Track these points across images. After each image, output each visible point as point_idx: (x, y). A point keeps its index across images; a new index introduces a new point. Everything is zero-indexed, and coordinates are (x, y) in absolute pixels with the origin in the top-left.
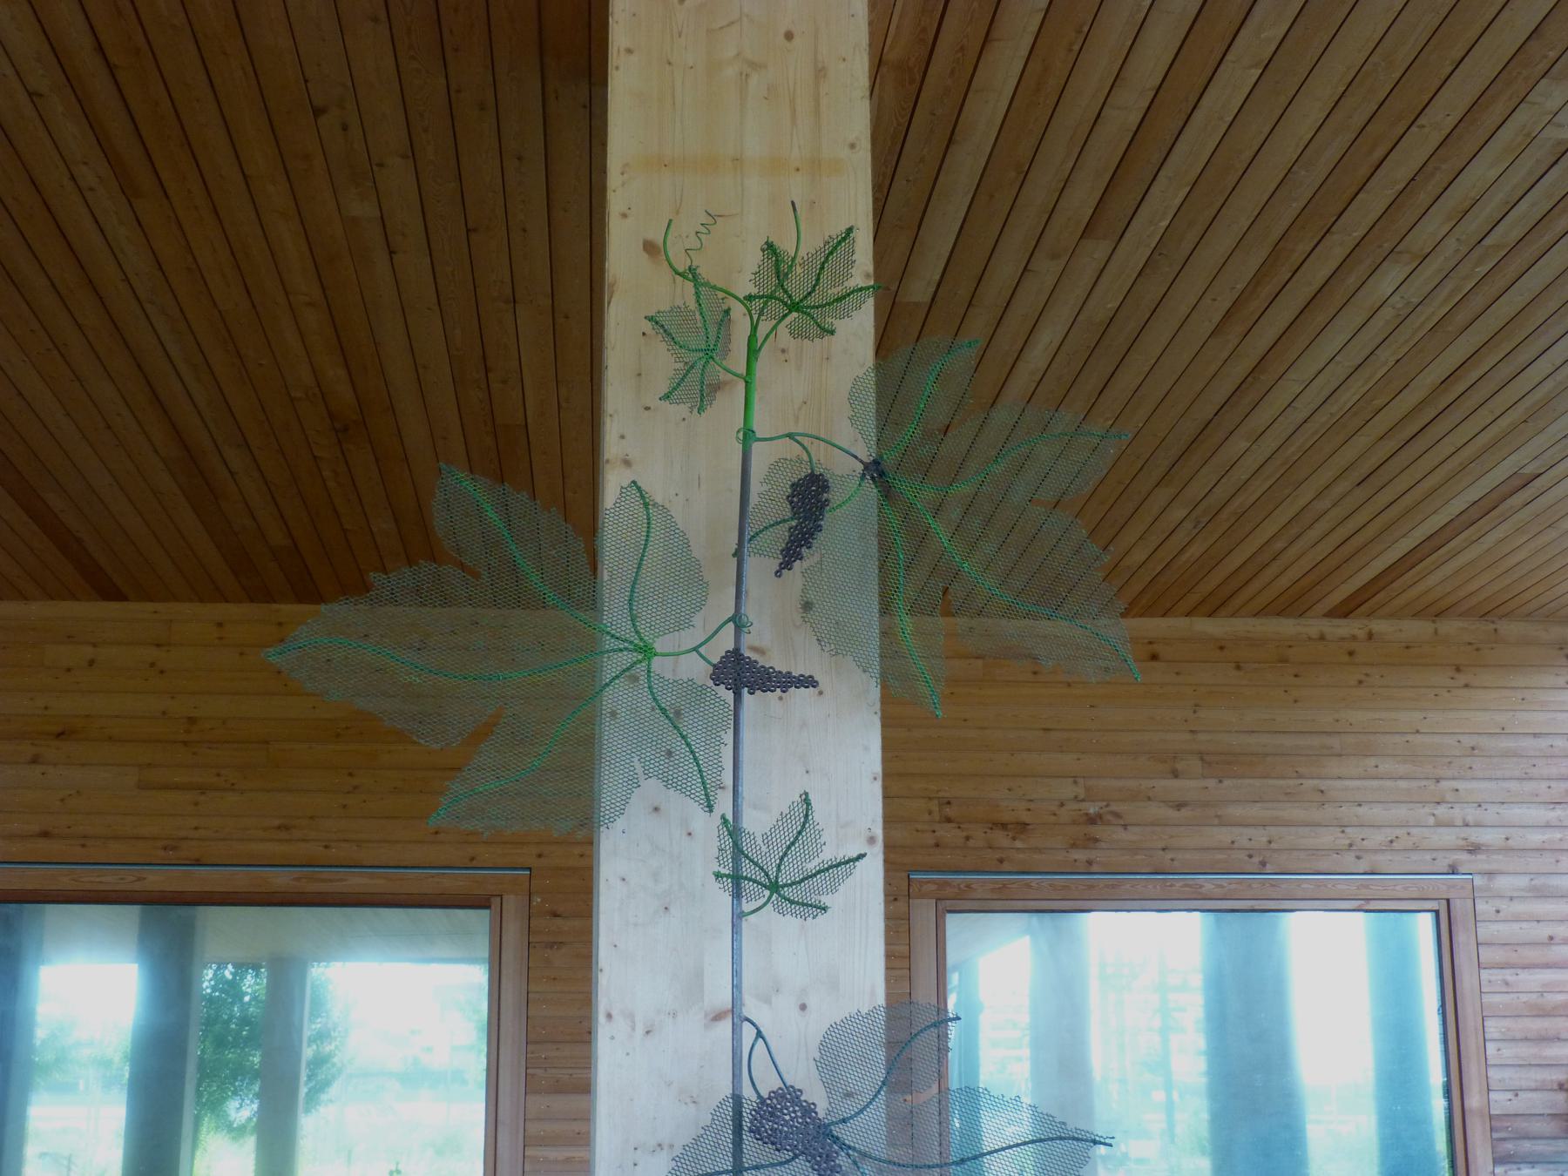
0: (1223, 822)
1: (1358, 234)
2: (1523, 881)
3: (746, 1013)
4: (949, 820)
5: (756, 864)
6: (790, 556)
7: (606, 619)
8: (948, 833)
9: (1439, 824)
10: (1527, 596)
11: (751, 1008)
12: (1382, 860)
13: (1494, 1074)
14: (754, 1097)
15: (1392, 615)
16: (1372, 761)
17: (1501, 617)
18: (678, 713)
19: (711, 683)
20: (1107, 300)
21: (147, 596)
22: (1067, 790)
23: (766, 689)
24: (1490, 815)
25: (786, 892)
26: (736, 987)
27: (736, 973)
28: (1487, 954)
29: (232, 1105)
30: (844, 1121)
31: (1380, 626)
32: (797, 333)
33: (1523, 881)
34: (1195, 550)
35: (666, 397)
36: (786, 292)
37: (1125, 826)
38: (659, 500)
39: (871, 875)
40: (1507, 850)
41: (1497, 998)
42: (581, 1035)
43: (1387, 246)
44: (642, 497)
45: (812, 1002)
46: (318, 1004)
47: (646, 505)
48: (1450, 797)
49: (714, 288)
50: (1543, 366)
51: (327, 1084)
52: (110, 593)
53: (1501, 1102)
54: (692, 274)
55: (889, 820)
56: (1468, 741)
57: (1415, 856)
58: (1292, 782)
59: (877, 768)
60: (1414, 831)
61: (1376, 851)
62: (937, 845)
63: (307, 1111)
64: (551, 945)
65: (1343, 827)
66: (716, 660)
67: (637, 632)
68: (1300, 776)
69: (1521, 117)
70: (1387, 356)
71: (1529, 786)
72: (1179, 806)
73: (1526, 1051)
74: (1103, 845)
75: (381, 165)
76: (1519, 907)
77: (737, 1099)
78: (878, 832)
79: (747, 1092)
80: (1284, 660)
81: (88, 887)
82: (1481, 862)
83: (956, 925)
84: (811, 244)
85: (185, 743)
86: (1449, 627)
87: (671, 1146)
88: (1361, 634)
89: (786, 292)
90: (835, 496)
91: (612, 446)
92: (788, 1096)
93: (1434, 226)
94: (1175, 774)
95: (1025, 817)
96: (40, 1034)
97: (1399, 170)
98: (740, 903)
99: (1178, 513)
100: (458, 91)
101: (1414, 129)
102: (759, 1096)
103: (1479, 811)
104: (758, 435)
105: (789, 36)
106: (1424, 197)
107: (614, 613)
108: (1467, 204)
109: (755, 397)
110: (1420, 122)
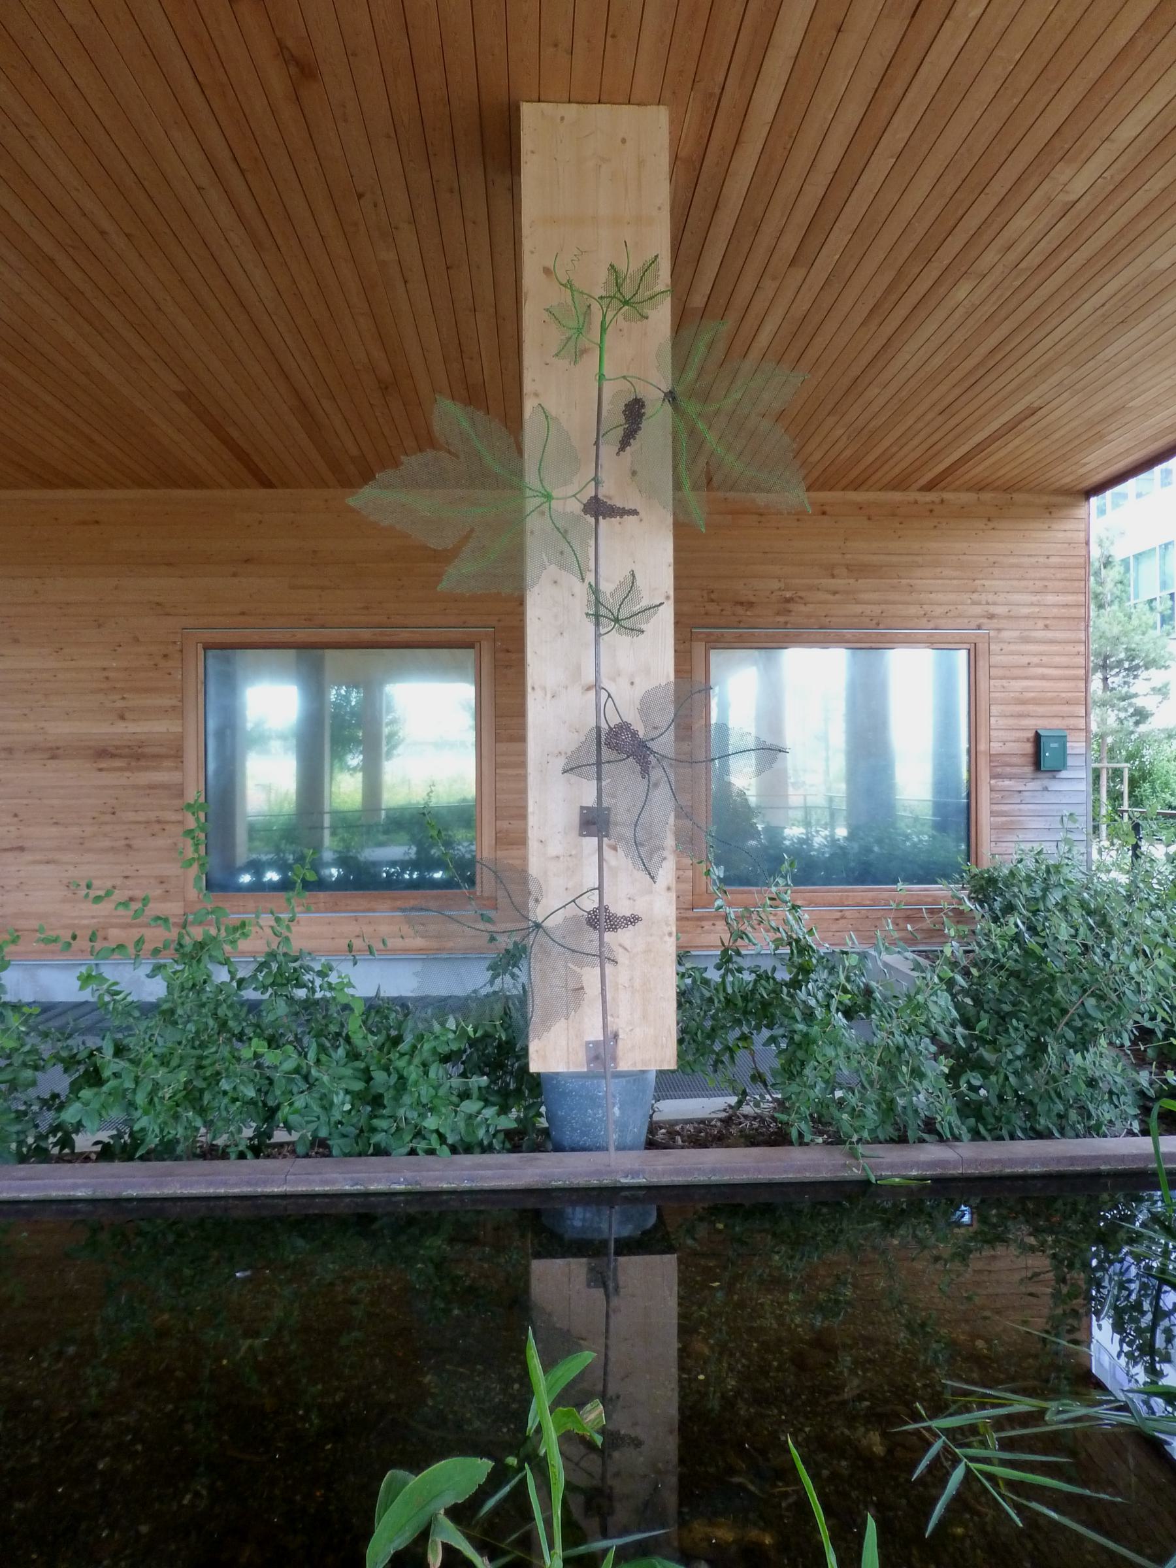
0: (858, 602)
1: (946, 262)
2: (1016, 634)
3: (602, 686)
4: (712, 601)
5: (607, 608)
6: (624, 444)
7: (527, 480)
8: (713, 608)
9: (974, 603)
10: (1030, 479)
11: (605, 683)
12: (942, 622)
13: (994, 733)
14: (607, 727)
15: (955, 490)
16: (939, 570)
17: (1014, 491)
18: (566, 531)
19: (582, 514)
20: (802, 306)
21: (285, 485)
22: (775, 585)
23: (611, 516)
24: (1001, 598)
25: (623, 623)
26: (597, 672)
27: (597, 665)
28: (994, 672)
29: (349, 757)
30: (652, 739)
31: (947, 496)
32: (627, 318)
33: (1016, 634)
34: (848, 453)
35: (557, 355)
36: (621, 294)
37: (805, 604)
38: (554, 414)
39: (666, 615)
40: (1009, 617)
41: (998, 695)
42: (520, 713)
43: (963, 269)
44: (544, 412)
45: (637, 681)
46: (390, 709)
47: (547, 417)
48: (979, 589)
49: (582, 293)
50: (1048, 342)
51: (395, 747)
52: (267, 484)
53: (996, 747)
54: (569, 285)
55: (676, 589)
56: (992, 559)
57: (959, 620)
58: (896, 581)
59: (671, 560)
60: (959, 607)
61: (938, 618)
62: (706, 614)
63: (388, 760)
64: (507, 667)
65: (921, 605)
66: (585, 501)
67: (543, 487)
68: (899, 577)
69: (1046, 186)
70: (960, 336)
71: (1023, 583)
72: (835, 593)
73: (1011, 722)
74: (793, 614)
75: (396, 228)
76: (1013, 647)
77: (598, 729)
78: (671, 593)
79: (604, 725)
80: (894, 515)
81: (267, 640)
82: (994, 623)
83: (716, 657)
84: (635, 266)
85: (312, 565)
86: (987, 496)
87: (566, 753)
88: (938, 500)
89: (621, 294)
90: (648, 410)
91: (528, 386)
92: (624, 727)
93: (990, 257)
94: (833, 576)
95: (753, 599)
96: (249, 726)
97: (972, 222)
98: (599, 629)
99: (839, 432)
100: (438, 181)
101: (982, 195)
102: (609, 727)
103: (995, 597)
104: (607, 377)
105: (624, 141)
106: (986, 238)
107: (531, 478)
108: (1011, 242)
109: (605, 357)
110: (986, 191)
